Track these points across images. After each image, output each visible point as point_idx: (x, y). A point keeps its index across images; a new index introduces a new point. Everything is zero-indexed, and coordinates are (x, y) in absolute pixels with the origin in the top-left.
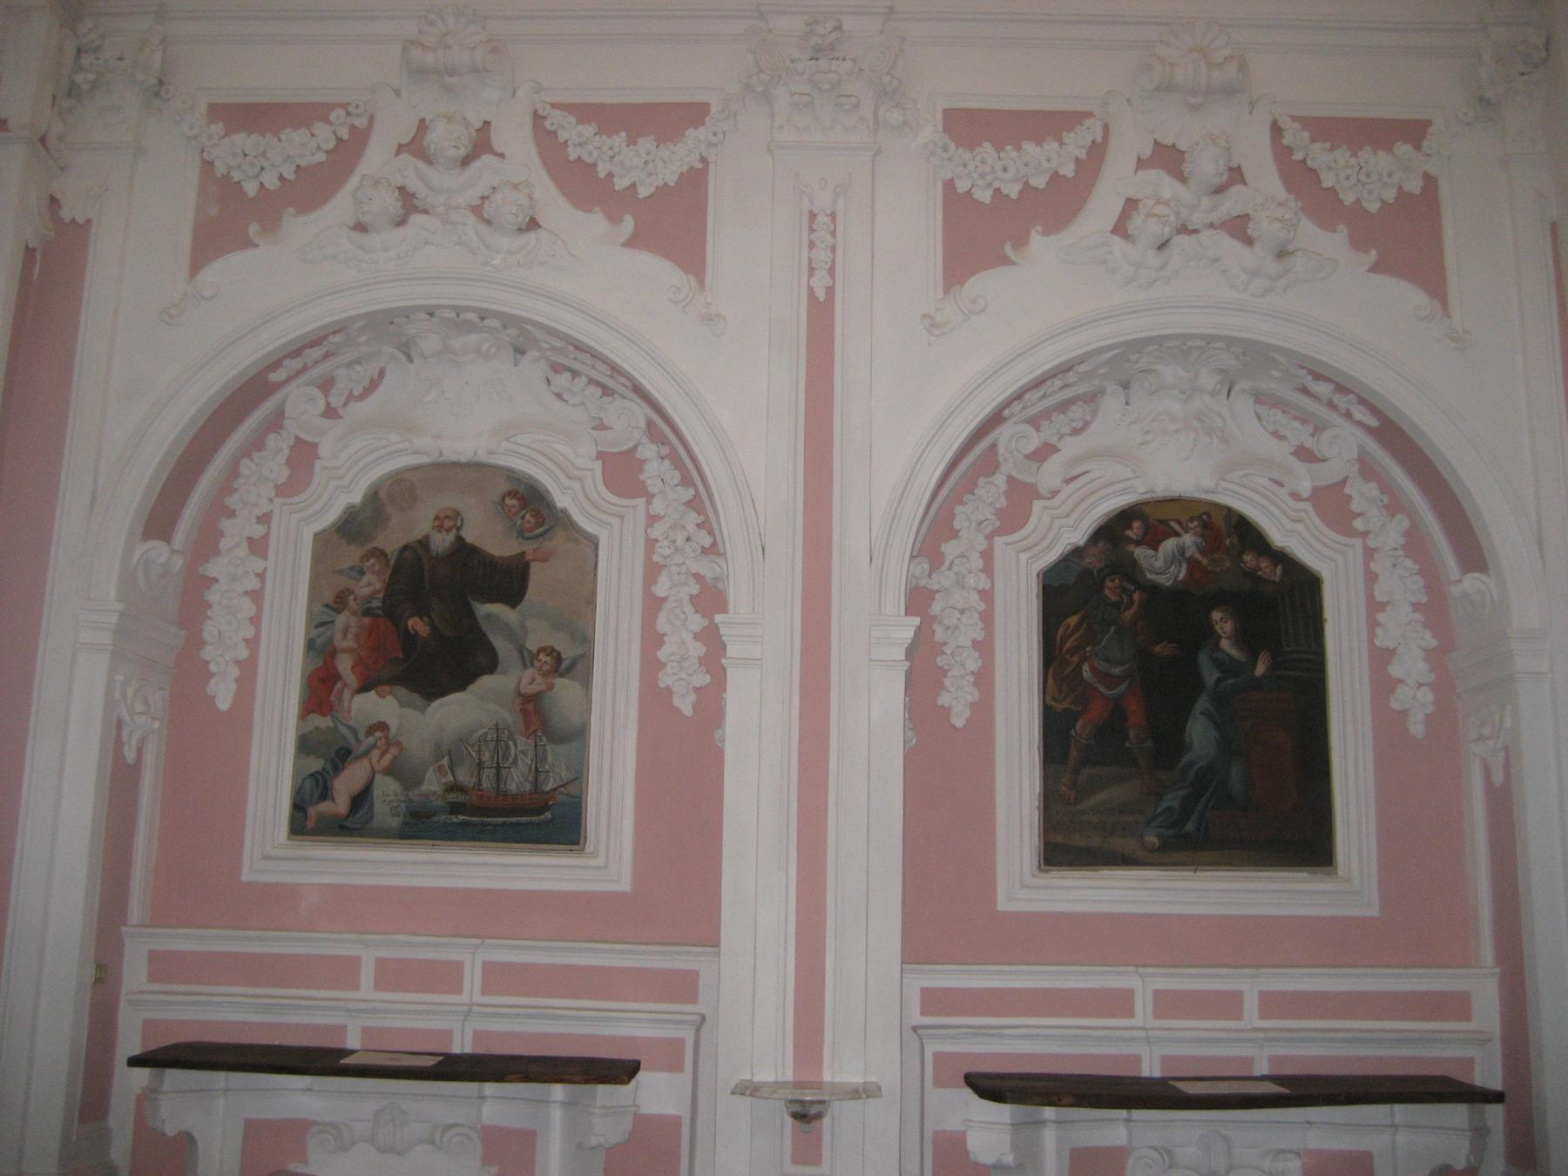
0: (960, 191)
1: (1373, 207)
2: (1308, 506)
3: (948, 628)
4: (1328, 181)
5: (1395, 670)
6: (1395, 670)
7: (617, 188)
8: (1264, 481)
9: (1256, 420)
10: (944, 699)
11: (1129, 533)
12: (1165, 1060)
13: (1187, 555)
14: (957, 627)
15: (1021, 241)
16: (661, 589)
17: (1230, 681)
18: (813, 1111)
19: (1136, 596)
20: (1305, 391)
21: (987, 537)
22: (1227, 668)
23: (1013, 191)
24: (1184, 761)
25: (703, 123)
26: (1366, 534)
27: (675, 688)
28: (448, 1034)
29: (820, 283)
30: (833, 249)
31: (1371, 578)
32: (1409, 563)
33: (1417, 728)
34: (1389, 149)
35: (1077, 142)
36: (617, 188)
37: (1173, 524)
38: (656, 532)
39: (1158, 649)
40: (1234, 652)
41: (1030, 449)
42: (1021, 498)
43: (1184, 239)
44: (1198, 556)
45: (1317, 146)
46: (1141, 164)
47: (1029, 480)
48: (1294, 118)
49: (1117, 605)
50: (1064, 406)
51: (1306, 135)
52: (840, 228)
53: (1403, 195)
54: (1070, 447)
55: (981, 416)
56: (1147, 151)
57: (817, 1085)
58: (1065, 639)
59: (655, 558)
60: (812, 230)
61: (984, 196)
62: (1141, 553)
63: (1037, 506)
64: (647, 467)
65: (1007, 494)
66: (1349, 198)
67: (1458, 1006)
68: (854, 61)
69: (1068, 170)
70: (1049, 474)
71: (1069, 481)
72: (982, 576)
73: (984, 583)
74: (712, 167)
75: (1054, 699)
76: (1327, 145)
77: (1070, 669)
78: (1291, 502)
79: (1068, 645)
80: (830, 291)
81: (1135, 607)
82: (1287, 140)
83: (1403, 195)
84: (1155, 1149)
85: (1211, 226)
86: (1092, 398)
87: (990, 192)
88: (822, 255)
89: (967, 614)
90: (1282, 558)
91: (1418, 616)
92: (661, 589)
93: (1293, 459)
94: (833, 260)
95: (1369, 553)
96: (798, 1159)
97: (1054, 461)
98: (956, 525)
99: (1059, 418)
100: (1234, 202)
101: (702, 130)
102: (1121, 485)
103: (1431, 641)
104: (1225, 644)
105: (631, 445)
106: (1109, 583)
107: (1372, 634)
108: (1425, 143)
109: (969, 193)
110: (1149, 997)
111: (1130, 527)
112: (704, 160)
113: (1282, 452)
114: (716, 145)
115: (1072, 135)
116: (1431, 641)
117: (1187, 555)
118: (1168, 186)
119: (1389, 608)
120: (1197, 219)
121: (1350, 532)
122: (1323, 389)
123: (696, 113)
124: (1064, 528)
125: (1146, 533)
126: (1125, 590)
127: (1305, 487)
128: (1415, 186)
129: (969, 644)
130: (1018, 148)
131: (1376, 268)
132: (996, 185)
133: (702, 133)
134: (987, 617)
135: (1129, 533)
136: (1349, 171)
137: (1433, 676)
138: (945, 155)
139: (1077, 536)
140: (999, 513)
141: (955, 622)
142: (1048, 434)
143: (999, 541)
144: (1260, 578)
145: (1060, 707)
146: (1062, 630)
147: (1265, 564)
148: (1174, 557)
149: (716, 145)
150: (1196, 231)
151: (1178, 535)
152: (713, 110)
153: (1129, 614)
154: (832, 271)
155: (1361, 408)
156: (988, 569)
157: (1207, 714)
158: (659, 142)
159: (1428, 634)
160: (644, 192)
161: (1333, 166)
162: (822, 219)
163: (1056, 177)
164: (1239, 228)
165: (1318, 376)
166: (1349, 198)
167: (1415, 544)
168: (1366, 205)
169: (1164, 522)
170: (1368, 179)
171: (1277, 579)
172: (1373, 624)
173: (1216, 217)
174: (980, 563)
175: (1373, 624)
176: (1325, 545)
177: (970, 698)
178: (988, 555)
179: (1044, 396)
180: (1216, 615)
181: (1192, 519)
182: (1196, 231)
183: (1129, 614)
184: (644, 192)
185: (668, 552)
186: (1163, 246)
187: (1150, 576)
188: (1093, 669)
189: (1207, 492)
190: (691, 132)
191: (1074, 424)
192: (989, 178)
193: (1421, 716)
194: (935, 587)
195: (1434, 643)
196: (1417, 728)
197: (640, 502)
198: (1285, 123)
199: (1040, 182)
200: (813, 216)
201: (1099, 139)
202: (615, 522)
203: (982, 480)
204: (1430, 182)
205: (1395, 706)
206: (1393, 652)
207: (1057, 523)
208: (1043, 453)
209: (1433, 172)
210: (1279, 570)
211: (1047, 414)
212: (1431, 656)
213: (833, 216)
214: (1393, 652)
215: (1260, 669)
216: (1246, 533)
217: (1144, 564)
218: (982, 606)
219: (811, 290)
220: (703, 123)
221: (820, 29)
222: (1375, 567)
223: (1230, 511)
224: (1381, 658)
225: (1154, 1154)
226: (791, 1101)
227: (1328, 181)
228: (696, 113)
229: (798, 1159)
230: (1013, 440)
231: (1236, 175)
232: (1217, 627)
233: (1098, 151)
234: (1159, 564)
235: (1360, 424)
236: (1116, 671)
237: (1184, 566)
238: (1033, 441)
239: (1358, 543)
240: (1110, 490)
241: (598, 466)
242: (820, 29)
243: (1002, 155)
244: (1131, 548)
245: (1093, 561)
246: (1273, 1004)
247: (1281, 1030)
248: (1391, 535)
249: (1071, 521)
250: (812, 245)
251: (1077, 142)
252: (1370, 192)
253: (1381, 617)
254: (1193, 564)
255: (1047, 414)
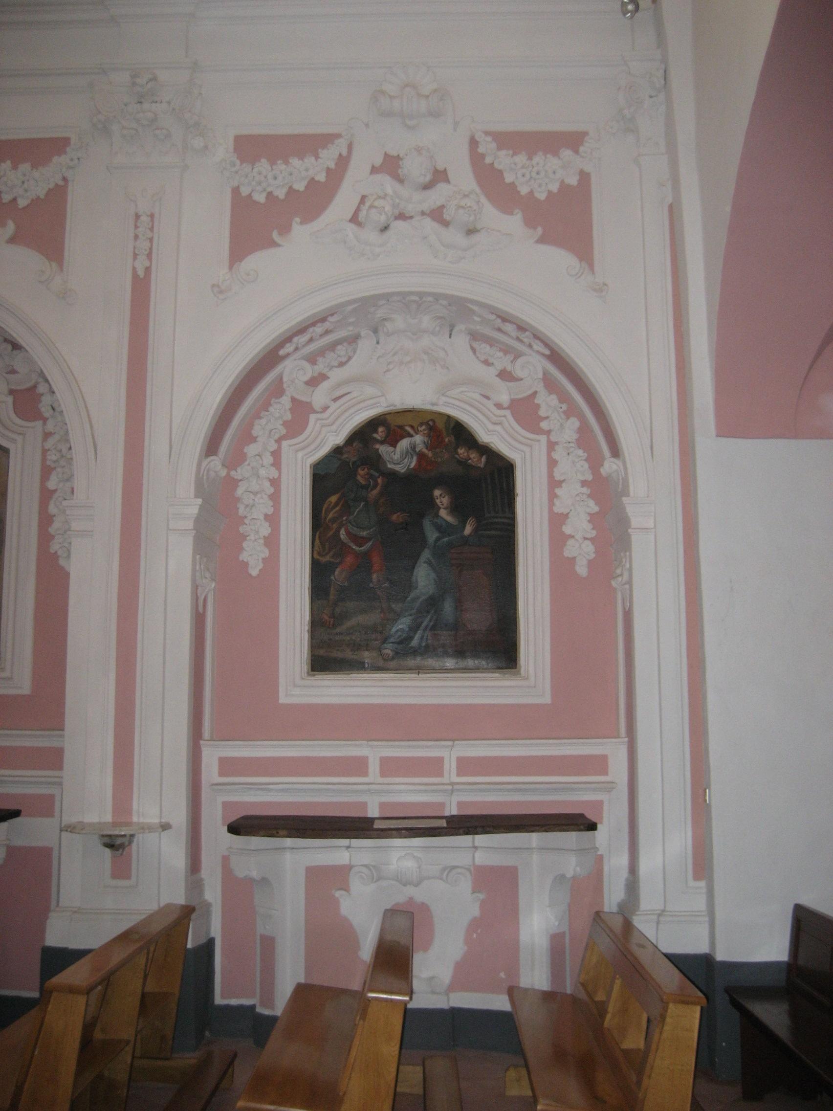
0: (244, 194)
1: (542, 196)
2: (508, 413)
3: (247, 506)
4: (509, 178)
5: (567, 529)
6: (567, 529)
7: (4, 201)
8: (477, 396)
9: (470, 353)
10: (244, 556)
11: (375, 435)
12: (460, 804)
13: (417, 450)
14: (253, 506)
15: (285, 229)
16: (51, 484)
17: (446, 539)
18: (119, 841)
19: (380, 480)
20: (499, 330)
21: (276, 441)
22: (443, 529)
23: (281, 193)
24: (412, 595)
25: (65, 153)
26: (548, 433)
27: (59, 553)
28: (365, 805)
29: (141, 265)
30: (151, 240)
31: (552, 463)
32: (580, 452)
33: (582, 569)
34: (556, 153)
35: (329, 156)
36: (4, 201)
37: (408, 429)
38: (49, 444)
39: (394, 517)
40: (449, 519)
41: (306, 378)
42: (301, 412)
43: (400, 224)
44: (425, 451)
45: (503, 153)
46: (374, 170)
47: (308, 400)
48: (487, 133)
49: (366, 487)
50: (332, 347)
51: (494, 145)
52: (156, 224)
53: (564, 187)
54: (336, 375)
55: (251, 356)
56: (378, 161)
57: (129, 824)
58: (328, 511)
59: (48, 463)
60: (136, 227)
61: (261, 198)
62: (383, 449)
63: (313, 417)
64: (43, 398)
65: (291, 410)
66: (524, 190)
67: (599, 764)
68: (169, 103)
69: (321, 177)
70: (319, 397)
71: (335, 400)
72: (273, 469)
73: (274, 473)
74: (70, 183)
75: (319, 554)
76: (511, 152)
77: (331, 533)
78: (494, 409)
79: (330, 516)
80: (148, 270)
81: (378, 488)
82: (481, 150)
83: (564, 187)
84: (365, 866)
85: (423, 213)
86: (354, 339)
87: (264, 195)
88: (144, 245)
89: (259, 496)
90: (486, 450)
91: (585, 490)
92: (51, 484)
93: (498, 380)
94: (151, 249)
95: (552, 446)
96: (115, 875)
97: (325, 385)
98: (254, 433)
99: (330, 356)
100: (438, 195)
101: (63, 157)
102: (372, 401)
103: (594, 508)
104: (443, 513)
105: (530, 392)
106: (361, 472)
107: (551, 504)
108: (581, 149)
109: (250, 196)
110: (378, 762)
111: (376, 431)
112: (65, 179)
113: (489, 374)
114: (71, 168)
115: (325, 151)
116: (594, 508)
117: (417, 450)
118: (387, 183)
119: (564, 485)
120: (410, 209)
121: (540, 432)
122: (509, 328)
123: (59, 145)
124: (330, 434)
125: (387, 436)
126: (371, 476)
127: (505, 399)
128: (573, 181)
129: (262, 517)
130: (286, 162)
131: (541, 240)
132: (269, 189)
133: (63, 159)
134: (275, 498)
135: (375, 435)
136: (524, 170)
137: (594, 533)
138: (233, 169)
139: (338, 438)
140: (285, 424)
141: (251, 502)
142: (321, 366)
143: (285, 444)
144: (470, 466)
145: (324, 560)
146: (325, 506)
147: (473, 455)
148: (407, 452)
149: (71, 168)
150: (411, 217)
151: (412, 436)
152: (72, 142)
153: (375, 492)
154: (149, 256)
155: (537, 341)
156: (277, 464)
157: (429, 563)
158: (34, 166)
159: (591, 503)
160: (22, 203)
161: (513, 167)
162: (144, 218)
163: (312, 182)
164: (437, 215)
165: (504, 320)
166: (524, 190)
167: (584, 438)
168: (537, 195)
169: (401, 427)
170: (542, 176)
171: (482, 466)
172: (552, 496)
173: (426, 207)
174: (271, 460)
175: (552, 496)
176: (516, 440)
177: (263, 556)
178: (276, 455)
179: (311, 340)
180: (437, 493)
181: (421, 424)
182: (411, 217)
183: (375, 492)
184: (22, 203)
185: (54, 458)
186: (385, 228)
187: (389, 466)
188: (348, 533)
189: (433, 404)
190: (55, 159)
191: (340, 359)
192: (264, 185)
193: (585, 562)
194: (240, 478)
195: (596, 509)
196: (582, 569)
197: (39, 424)
198: (479, 136)
199: (300, 186)
200: (137, 217)
201: (345, 153)
202: (527, 449)
203: (273, 400)
204: (584, 177)
205: (567, 554)
206: (566, 516)
207: (324, 430)
208: (314, 382)
209: (588, 168)
210: (484, 459)
211: (322, 352)
212: (593, 518)
213: (152, 216)
214: (566, 516)
215: (468, 530)
216: (460, 433)
217: (386, 457)
218: (272, 490)
219: (134, 269)
220: (65, 153)
221: (138, 81)
222: (555, 456)
223: (449, 417)
224: (557, 521)
225: (364, 870)
226: (103, 836)
227: (509, 178)
228: (59, 145)
229: (115, 875)
230: (293, 371)
231: (440, 176)
232: (438, 501)
233: (343, 162)
234: (397, 457)
235: (538, 352)
236: (364, 534)
237: (415, 458)
238: (309, 371)
239: (543, 439)
240: (362, 405)
241: (10, 399)
242: (138, 81)
243: (274, 167)
244: (377, 446)
245: (351, 456)
246: (466, 766)
247: (489, 783)
248: (569, 431)
249: (334, 427)
250: (136, 237)
251: (329, 156)
252: (540, 186)
253: (558, 491)
254: (421, 456)
255: (322, 352)
